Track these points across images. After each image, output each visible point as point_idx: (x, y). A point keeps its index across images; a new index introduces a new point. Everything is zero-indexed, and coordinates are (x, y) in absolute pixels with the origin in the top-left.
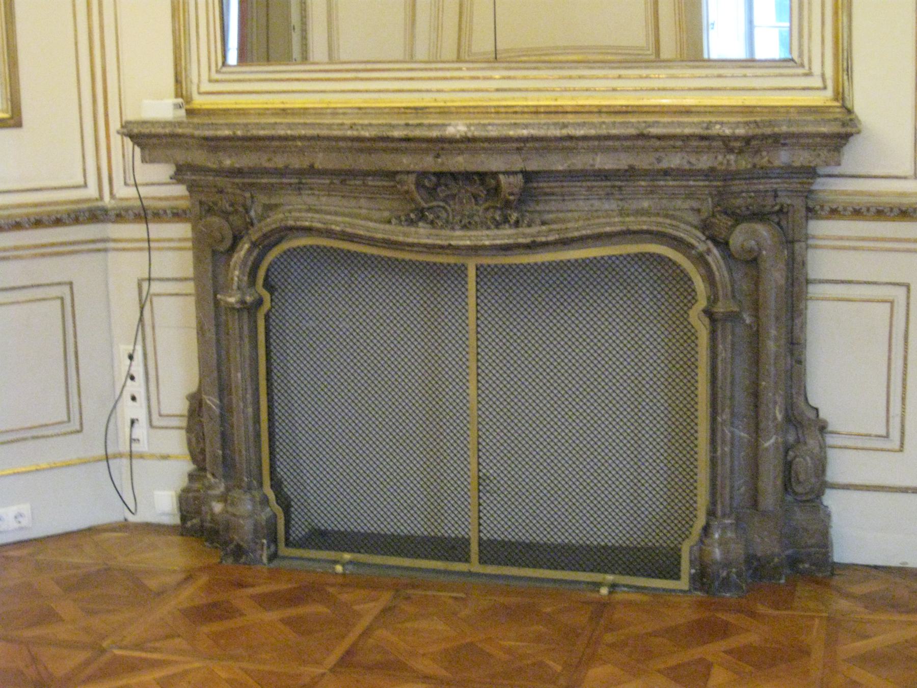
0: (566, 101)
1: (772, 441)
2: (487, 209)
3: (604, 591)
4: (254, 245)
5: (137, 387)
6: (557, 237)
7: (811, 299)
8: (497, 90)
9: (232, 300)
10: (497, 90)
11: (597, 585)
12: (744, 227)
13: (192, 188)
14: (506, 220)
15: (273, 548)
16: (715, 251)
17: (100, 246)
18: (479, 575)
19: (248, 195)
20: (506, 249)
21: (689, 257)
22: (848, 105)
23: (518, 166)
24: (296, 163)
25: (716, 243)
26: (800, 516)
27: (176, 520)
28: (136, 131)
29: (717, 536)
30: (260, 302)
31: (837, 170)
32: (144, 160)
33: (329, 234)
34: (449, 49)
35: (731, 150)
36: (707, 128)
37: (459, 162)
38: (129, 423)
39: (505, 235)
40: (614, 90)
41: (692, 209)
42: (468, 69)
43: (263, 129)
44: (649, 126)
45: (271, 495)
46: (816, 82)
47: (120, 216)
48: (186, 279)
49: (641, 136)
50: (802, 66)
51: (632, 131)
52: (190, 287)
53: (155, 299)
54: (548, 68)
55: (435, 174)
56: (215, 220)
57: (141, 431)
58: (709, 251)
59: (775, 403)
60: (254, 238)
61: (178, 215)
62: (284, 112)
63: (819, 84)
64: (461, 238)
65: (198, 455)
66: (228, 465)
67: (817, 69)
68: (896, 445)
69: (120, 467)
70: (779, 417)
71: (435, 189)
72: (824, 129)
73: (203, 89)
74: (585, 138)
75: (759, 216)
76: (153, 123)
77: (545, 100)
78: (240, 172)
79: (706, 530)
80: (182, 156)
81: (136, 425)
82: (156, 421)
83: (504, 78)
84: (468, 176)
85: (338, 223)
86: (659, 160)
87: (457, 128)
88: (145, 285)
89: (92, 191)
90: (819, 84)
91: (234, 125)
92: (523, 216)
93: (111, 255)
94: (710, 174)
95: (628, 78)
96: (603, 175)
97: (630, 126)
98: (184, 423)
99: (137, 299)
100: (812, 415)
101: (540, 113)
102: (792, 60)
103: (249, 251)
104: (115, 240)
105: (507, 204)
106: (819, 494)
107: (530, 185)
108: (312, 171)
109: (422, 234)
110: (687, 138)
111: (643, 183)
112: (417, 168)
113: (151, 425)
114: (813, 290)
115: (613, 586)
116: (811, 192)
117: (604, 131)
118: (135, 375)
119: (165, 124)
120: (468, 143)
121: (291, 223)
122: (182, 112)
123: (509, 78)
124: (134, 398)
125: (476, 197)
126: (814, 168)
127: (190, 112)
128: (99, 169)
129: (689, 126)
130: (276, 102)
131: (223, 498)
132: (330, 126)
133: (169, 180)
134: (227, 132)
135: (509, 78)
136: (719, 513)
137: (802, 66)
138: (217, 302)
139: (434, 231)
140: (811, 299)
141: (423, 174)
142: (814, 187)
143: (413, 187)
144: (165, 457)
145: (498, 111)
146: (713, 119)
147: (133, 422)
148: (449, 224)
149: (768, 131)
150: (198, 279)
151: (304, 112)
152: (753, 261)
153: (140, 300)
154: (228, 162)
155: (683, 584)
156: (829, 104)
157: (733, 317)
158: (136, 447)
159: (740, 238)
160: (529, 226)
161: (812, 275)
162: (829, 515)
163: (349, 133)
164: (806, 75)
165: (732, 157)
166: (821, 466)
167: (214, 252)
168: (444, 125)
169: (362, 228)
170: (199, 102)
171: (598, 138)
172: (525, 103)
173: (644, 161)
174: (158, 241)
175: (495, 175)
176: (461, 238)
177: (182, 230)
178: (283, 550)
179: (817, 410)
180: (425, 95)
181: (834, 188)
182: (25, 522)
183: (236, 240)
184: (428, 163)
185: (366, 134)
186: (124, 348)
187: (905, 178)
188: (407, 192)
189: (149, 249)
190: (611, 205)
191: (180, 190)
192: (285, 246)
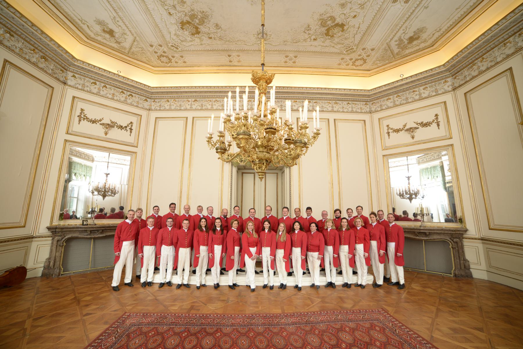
37: (422, 231)
152: (457, 243)
155: (452, 275)
166: (469, 266)
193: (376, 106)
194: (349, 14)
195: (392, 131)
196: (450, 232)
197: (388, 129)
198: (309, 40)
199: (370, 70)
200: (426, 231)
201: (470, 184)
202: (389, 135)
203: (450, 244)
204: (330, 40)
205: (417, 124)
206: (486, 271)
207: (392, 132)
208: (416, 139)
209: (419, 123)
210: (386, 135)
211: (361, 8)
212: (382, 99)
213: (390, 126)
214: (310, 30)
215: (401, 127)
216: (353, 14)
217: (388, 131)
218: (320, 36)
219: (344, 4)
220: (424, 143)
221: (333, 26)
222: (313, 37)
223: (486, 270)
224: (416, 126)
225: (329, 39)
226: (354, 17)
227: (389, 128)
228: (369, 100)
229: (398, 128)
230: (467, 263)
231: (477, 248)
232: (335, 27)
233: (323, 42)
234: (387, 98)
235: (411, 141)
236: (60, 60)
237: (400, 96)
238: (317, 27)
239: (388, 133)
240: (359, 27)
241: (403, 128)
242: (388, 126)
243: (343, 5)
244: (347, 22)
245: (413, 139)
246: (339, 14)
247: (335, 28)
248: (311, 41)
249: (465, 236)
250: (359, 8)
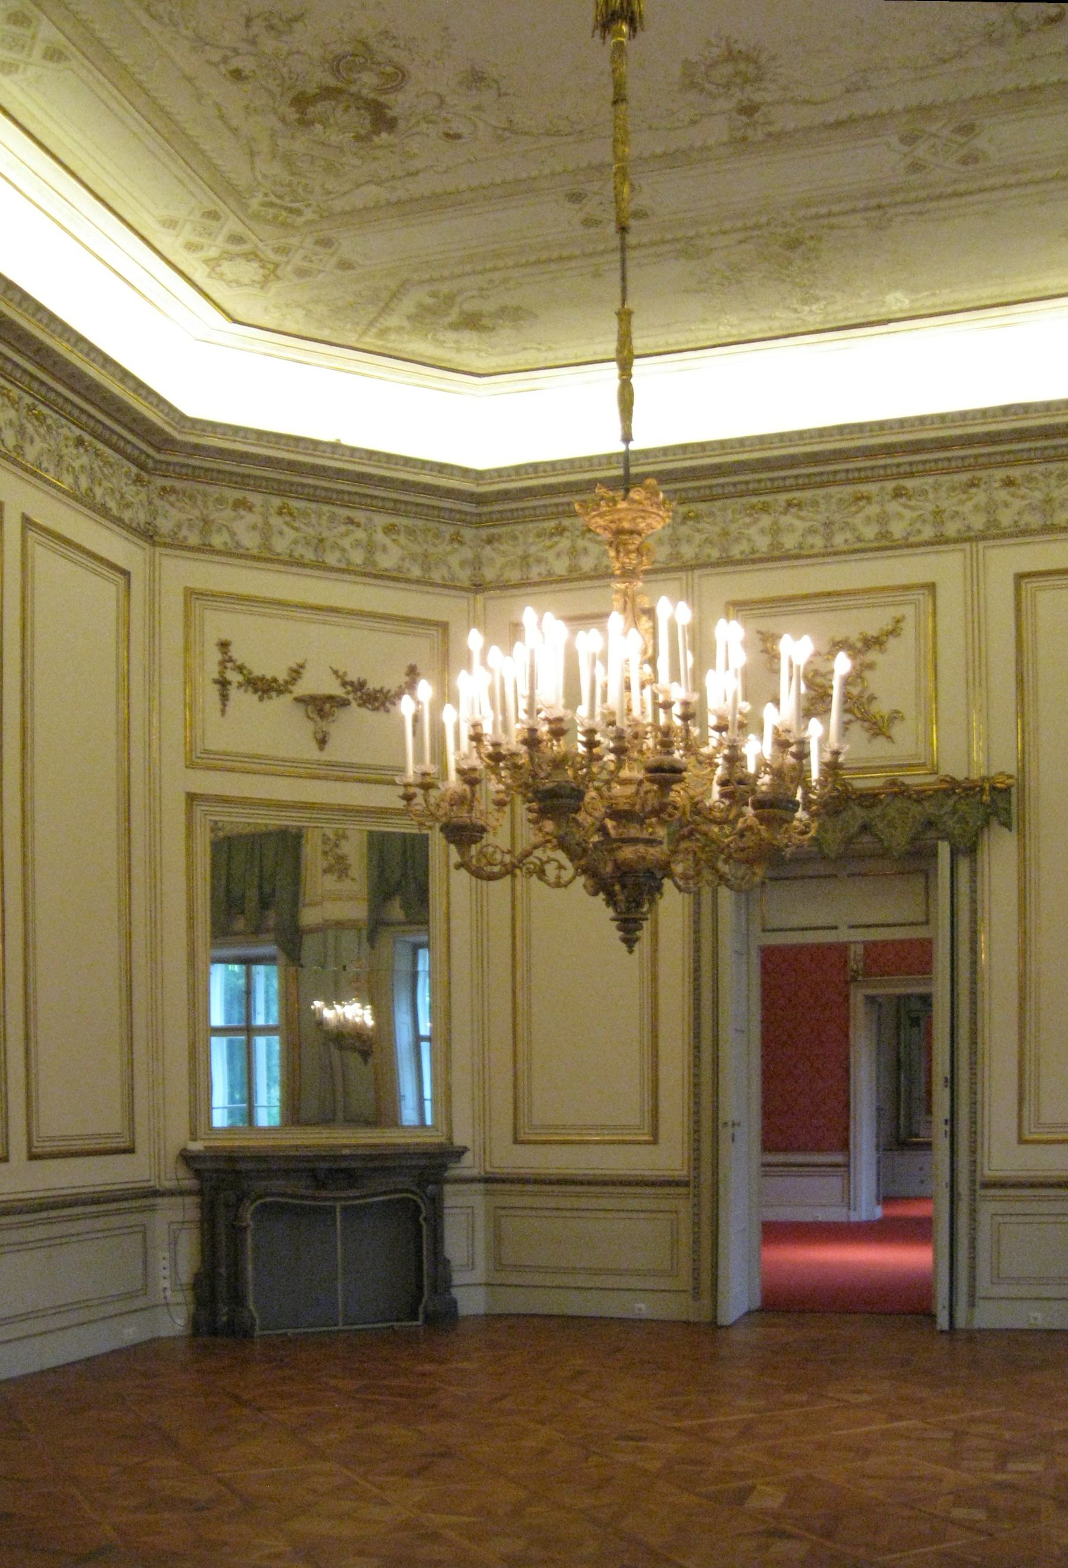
17: (152, 1208)
39: (352, 1193)
61: (189, 1193)
84: (342, 1170)
89: (152, 1183)
193: (184, 516)
194: (449, 116)
195: (240, 678)
197: (223, 664)
198: (216, 56)
199: (235, 321)
200: (354, 1165)
202: (224, 697)
204: (279, 125)
205: (344, 684)
207: (240, 685)
208: (335, 752)
209: (352, 684)
210: (214, 691)
211: (500, 132)
212: (214, 491)
213: (234, 652)
214: (280, 33)
215: (282, 676)
216: (457, 126)
217: (222, 673)
218: (273, 84)
219: (482, 79)
220: (361, 781)
221: (361, 98)
222: (246, 64)
224: (338, 691)
225: (283, 120)
226: (448, 135)
227: (231, 660)
228: (150, 464)
229: (269, 677)
232: (358, 108)
233: (247, 107)
234: (238, 494)
235: (310, 751)
237: (291, 514)
238: (316, 53)
239: (223, 684)
240: (417, 173)
241: (286, 682)
242: (224, 645)
243: (476, 79)
244: (415, 130)
245: (321, 749)
246: (431, 89)
247: (353, 110)
248: (215, 65)
249: (453, 1172)
250: (495, 128)
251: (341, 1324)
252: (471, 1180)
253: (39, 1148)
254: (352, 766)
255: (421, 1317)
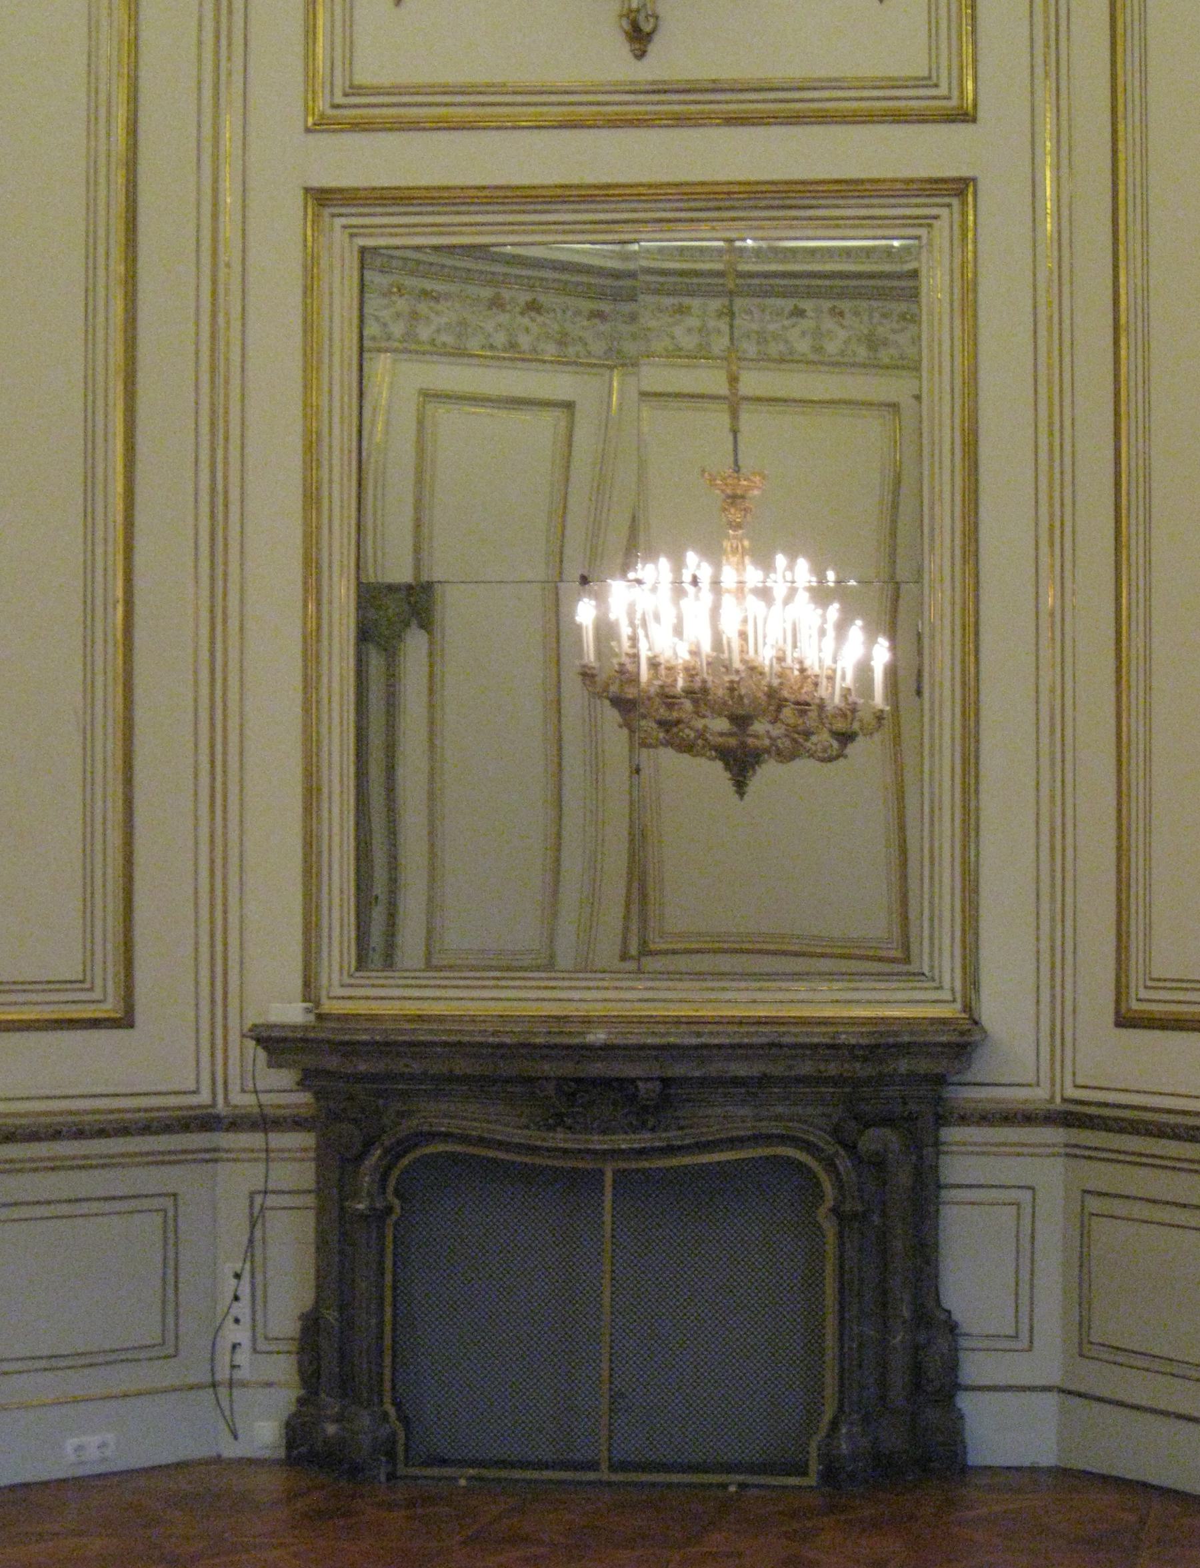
0: (707, 1012)
1: (899, 1338)
2: (626, 1115)
3: (732, 1489)
4: (386, 1152)
5: (242, 1309)
6: (693, 1141)
7: (944, 1203)
8: (640, 1000)
9: (361, 1206)
10: (640, 1000)
11: (724, 1486)
12: (871, 1132)
13: (319, 1095)
14: (644, 1125)
15: (390, 1468)
16: (842, 1152)
17: (212, 1156)
18: (609, 1484)
19: (381, 1102)
20: (641, 1152)
21: (820, 1160)
22: (977, 1018)
23: (657, 1073)
24: (436, 1068)
25: (845, 1146)
26: (932, 1415)
27: (281, 1453)
28: (265, 1034)
29: (844, 1431)
30: (389, 1210)
31: (968, 1077)
32: (270, 1066)
33: (464, 1139)
34: (607, 947)
35: (855, 1058)
36: (834, 1038)
37: (597, 1069)
38: (229, 1347)
39: (644, 1139)
40: (754, 1001)
41: (824, 1115)
42: (612, 979)
43: (402, 1035)
44: (780, 1036)
45: (392, 1411)
46: (946, 995)
47: (236, 1123)
48: (310, 1192)
49: (771, 1045)
50: (933, 980)
51: (764, 1040)
52: (310, 1200)
53: (268, 1213)
54: (692, 980)
55: (572, 1080)
56: (346, 1127)
57: (243, 1357)
58: (837, 1153)
59: (902, 1299)
60: (387, 1143)
61: (298, 1124)
62: (420, 1018)
63: (949, 997)
64: (599, 1142)
65: (310, 1378)
66: (346, 1386)
67: (947, 984)
68: (1026, 1345)
69: (223, 1391)
70: (906, 1314)
71: (573, 1094)
72: (944, 1039)
73: (332, 994)
74: (719, 1047)
75: (887, 1121)
76: (283, 1027)
77: (686, 1011)
78: (373, 1078)
79: (834, 1425)
80: (310, 1061)
81: (238, 1350)
82: (262, 1345)
83: (646, 989)
84: (607, 1083)
85: (476, 1129)
86: (790, 1068)
87: (598, 1036)
88: (259, 1199)
89: (204, 1098)
90: (949, 997)
91: (374, 1030)
92: (660, 1122)
93: (220, 1165)
94: (837, 1081)
95: (768, 990)
96: (736, 1082)
97: (763, 1036)
98: (293, 1347)
99: (247, 1211)
100: (943, 1317)
101: (681, 1023)
102: (923, 974)
103: (380, 1159)
104: (227, 1151)
105: (645, 1108)
106: (951, 1397)
107: (667, 1091)
108: (452, 1078)
109: (560, 1139)
110: (816, 1046)
111: (776, 1090)
112: (559, 1074)
113: (255, 1350)
114: (945, 1194)
115: (743, 1486)
116: (940, 1098)
117: (737, 1040)
118: (241, 1296)
119: (294, 1028)
120: (607, 1050)
121: (426, 1128)
122: (312, 1017)
123: (651, 988)
124: (237, 1321)
125: (615, 1103)
126: (944, 1076)
127: (320, 1017)
128: (213, 1074)
129: (818, 1036)
130: (412, 1008)
131: (339, 1419)
132: (471, 1033)
133: (295, 1087)
134: (365, 1037)
135: (651, 988)
136: (847, 1410)
137: (933, 980)
138: (342, 1208)
139: (570, 1136)
140: (944, 1203)
141: (565, 1080)
142: (945, 1095)
143: (552, 1093)
144: (269, 1385)
145: (641, 1020)
146: (841, 1030)
147: (235, 1347)
148: (587, 1129)
149: (891, 1040)
150: (319, 1191)
151: (441, 1019)
152: (878, 1164)
153: (251, 1214)
154: (362, 1067)
155: (812, 1480)
156: (958, 1015)
157: (864, 1216)
158: (238, 1375)
159: (872, 1140)
160: (665, 1130)
161: (943, 1181)
162: (962, 1417)
163: (491, 1039)
164: (937, 988)
165: (858, 1065)
166: (952, 1366)
167: (343, 1160)
168: (583, 1033)
169: (502, 1132)
170: (328, 1007)
171: (732, 1046)
172: (666, 1013)
173: (777, 1070)
174: (256, 1160)
175: (633, 1081)
176: (599, 1142)
177: (306, 1139)
178: (402, 1470)
179: (949, 1312)
180: (566, 1004)
181: (966, 1095)
182: (108, 1453)
183: (368, 1145)
184: (568, 1069)
185: (508, 1040)
186: (229, 1268)
187: (1029, 1085)
188: (546, 1097)
189: (267, 1160)
190: (745, 1111)
191: (305, 1097)
192: (417, 1153)
196: (832, 1069)
201: (1050, 599)
203: (823, 1177)
206: (1051, 1400)
220: (732, 121)
223: (1056, 1379)
230: (942, 1343)
231: (87, 985)
236: (926, 896)
245: (640, 55)
251: (604, 1466)
252: (1027, 1118)
253: (1140, 1000)
254: (716, 87)
255: (814, 1467)
